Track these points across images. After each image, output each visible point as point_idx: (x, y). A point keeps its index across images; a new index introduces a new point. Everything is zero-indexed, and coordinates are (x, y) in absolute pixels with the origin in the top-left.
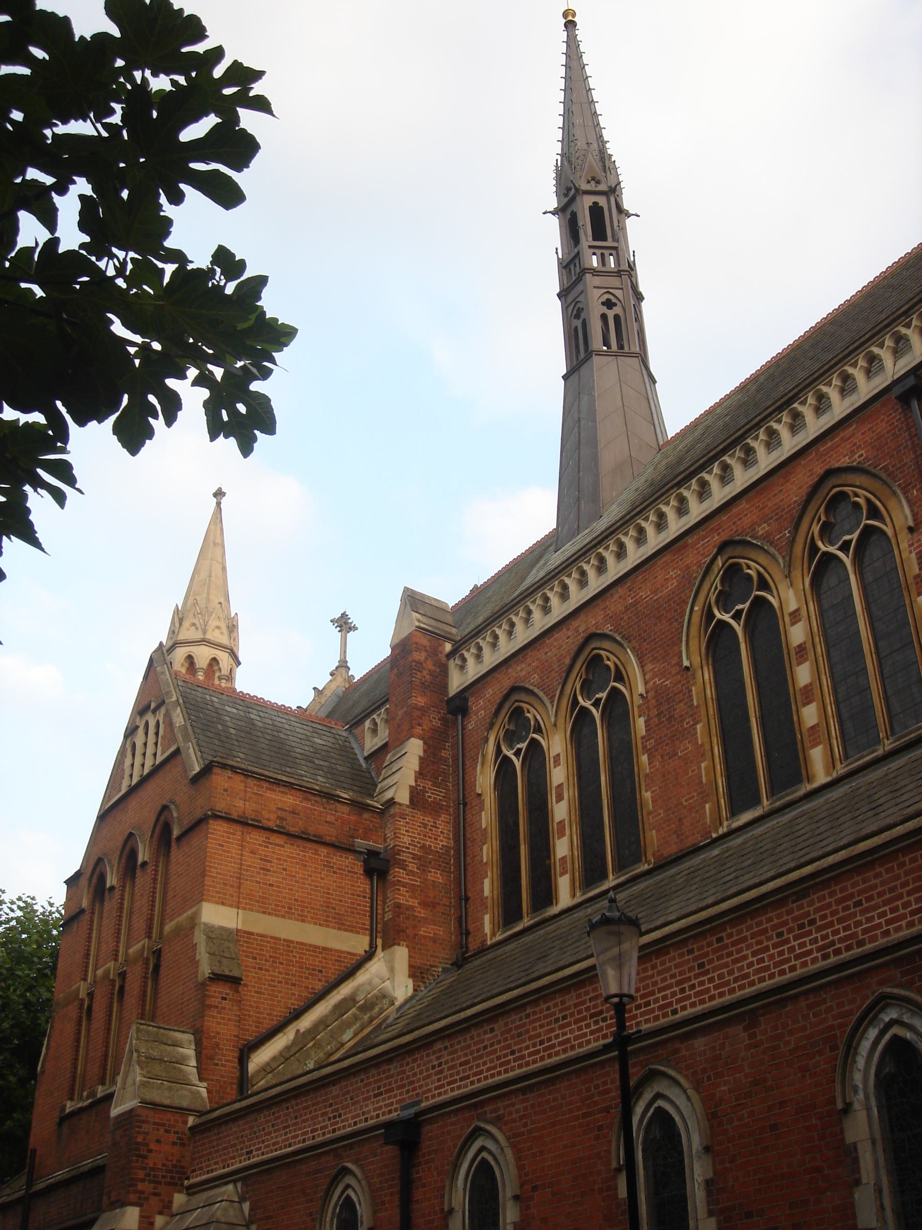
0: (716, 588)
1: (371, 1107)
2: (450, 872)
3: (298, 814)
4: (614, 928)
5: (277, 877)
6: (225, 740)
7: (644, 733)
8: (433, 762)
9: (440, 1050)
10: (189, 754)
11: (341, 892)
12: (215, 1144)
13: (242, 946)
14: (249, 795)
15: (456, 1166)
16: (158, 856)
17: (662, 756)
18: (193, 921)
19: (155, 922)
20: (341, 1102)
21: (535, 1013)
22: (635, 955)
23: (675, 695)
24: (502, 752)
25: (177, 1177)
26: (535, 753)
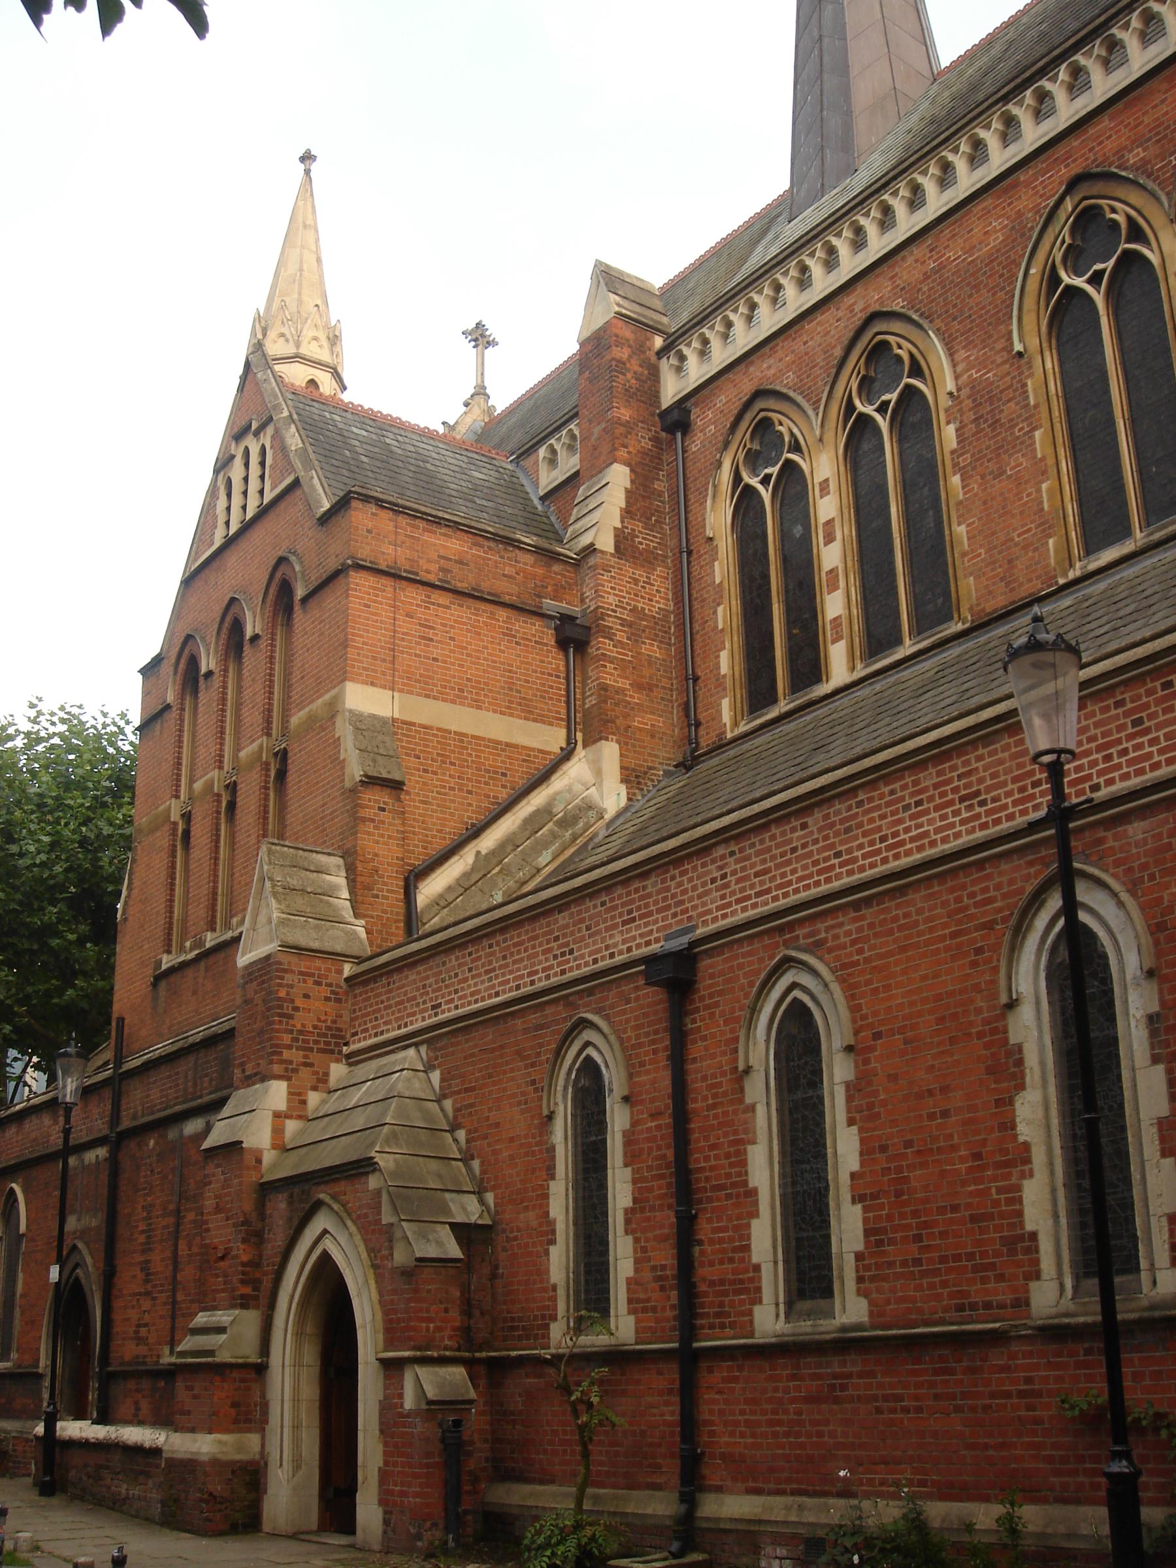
0: (1063, 242)
1: (618, 938)
2: (670, 645)
3: (467, 565)
4: (1047, 657)
5: (442, 649)
6: (357, 470)
7: (954, 445)
8: (644, 497)
9: (723, 857)
10: (312, 487)
11: (527, 670)
12: (384, 997)
13: (401, 741)
14: (401, 538)
15: (754, 1010)
16: (274, 627)
17: (983, 477)
18: (334, 709)
19: (275, 714)
20: (572, 934)
21: (870, 800)
22: (1074, 695)
23: (1001, 392)
24: (741, 480)
25: (333, 1042)
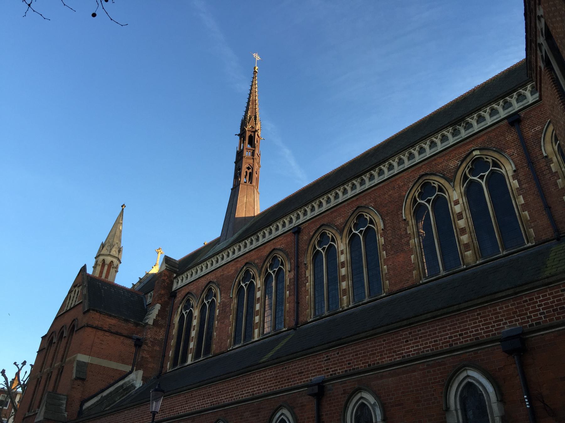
18: (75, 358)
26: (190, 314)
